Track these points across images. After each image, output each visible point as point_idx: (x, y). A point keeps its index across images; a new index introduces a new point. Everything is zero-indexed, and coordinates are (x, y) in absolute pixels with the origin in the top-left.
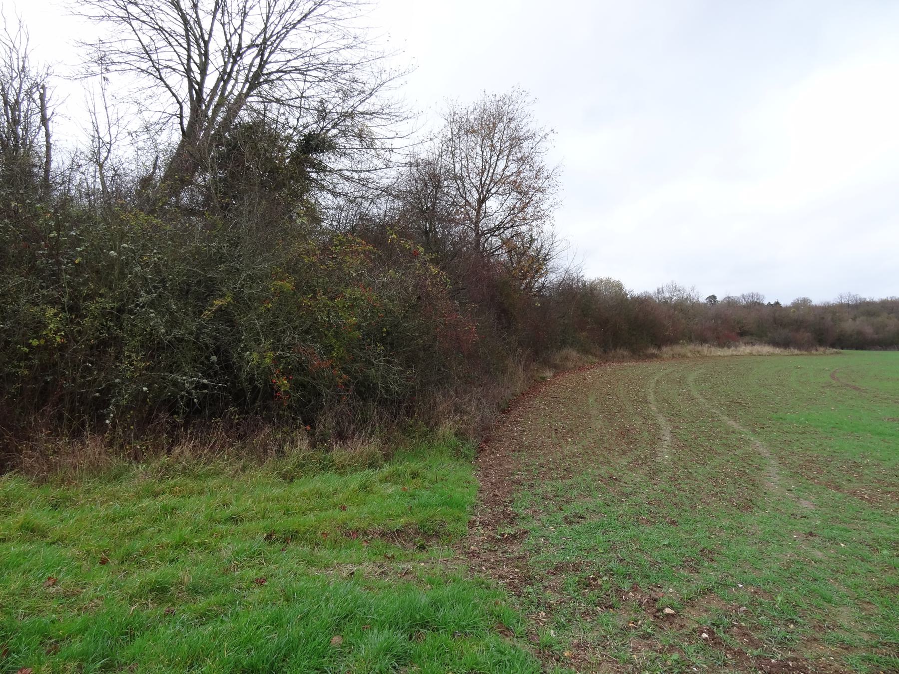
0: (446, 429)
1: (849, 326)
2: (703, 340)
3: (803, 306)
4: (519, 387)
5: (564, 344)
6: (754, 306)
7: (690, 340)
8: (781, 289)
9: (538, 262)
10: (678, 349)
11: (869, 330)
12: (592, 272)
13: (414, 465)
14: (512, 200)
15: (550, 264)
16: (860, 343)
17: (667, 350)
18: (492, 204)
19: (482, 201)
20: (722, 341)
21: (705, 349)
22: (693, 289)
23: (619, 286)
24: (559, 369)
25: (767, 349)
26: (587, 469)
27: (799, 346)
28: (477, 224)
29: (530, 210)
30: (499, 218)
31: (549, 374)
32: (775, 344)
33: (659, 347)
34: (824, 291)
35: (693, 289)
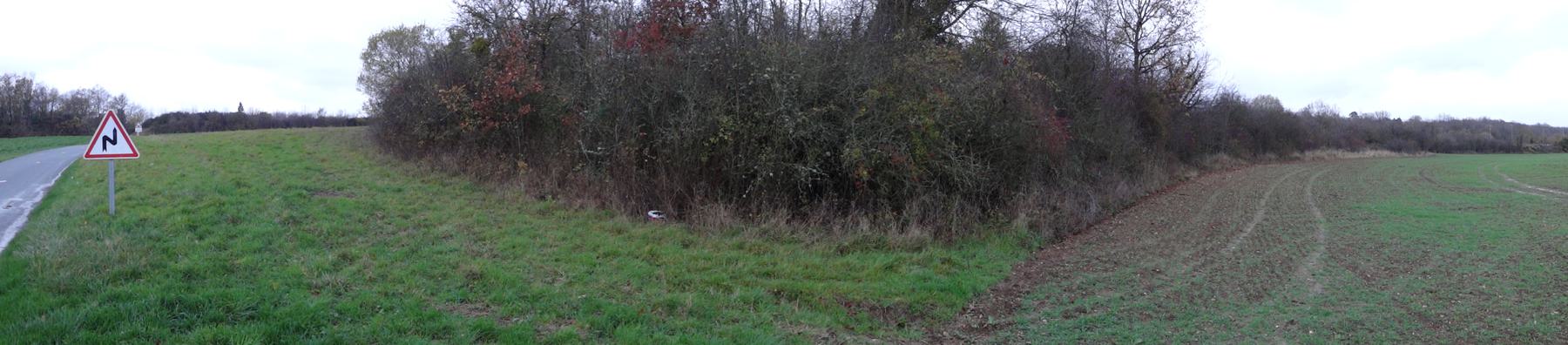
0: (1021, 221)
1: (1441, 136)
2: (1339, 146)
3: (1415, 121)
4: (1155, 185)
5: (1217, 149)
6: (1383, 121)
7: (1329, 146)
8: (1401, 111)
9: (1195, 79)
10: (1318, 153)
11: (1453, 140)
12: (1249, 91)
13: (972, 251)
14: (1165, 22)
15: (1205, 80)
16: (1447, 148)
17: (1309, 154)
18: (1148, 26)
19: (1140, 24)
20: (1353, 146)
21: (1340, 154)
22: (241, 107)
23: (1277, 102)
24: (1204, 170)
25: (1386, 153)
26: (1160, 245)
27: (1408, 150)
28: (1136, 44)
29: (1181, 32)
30: (1154, 37)
31: (1194, 174)
32: (1392, 149)
33: (1302, 151)
34: (1430, 112)
35: (241, 107)
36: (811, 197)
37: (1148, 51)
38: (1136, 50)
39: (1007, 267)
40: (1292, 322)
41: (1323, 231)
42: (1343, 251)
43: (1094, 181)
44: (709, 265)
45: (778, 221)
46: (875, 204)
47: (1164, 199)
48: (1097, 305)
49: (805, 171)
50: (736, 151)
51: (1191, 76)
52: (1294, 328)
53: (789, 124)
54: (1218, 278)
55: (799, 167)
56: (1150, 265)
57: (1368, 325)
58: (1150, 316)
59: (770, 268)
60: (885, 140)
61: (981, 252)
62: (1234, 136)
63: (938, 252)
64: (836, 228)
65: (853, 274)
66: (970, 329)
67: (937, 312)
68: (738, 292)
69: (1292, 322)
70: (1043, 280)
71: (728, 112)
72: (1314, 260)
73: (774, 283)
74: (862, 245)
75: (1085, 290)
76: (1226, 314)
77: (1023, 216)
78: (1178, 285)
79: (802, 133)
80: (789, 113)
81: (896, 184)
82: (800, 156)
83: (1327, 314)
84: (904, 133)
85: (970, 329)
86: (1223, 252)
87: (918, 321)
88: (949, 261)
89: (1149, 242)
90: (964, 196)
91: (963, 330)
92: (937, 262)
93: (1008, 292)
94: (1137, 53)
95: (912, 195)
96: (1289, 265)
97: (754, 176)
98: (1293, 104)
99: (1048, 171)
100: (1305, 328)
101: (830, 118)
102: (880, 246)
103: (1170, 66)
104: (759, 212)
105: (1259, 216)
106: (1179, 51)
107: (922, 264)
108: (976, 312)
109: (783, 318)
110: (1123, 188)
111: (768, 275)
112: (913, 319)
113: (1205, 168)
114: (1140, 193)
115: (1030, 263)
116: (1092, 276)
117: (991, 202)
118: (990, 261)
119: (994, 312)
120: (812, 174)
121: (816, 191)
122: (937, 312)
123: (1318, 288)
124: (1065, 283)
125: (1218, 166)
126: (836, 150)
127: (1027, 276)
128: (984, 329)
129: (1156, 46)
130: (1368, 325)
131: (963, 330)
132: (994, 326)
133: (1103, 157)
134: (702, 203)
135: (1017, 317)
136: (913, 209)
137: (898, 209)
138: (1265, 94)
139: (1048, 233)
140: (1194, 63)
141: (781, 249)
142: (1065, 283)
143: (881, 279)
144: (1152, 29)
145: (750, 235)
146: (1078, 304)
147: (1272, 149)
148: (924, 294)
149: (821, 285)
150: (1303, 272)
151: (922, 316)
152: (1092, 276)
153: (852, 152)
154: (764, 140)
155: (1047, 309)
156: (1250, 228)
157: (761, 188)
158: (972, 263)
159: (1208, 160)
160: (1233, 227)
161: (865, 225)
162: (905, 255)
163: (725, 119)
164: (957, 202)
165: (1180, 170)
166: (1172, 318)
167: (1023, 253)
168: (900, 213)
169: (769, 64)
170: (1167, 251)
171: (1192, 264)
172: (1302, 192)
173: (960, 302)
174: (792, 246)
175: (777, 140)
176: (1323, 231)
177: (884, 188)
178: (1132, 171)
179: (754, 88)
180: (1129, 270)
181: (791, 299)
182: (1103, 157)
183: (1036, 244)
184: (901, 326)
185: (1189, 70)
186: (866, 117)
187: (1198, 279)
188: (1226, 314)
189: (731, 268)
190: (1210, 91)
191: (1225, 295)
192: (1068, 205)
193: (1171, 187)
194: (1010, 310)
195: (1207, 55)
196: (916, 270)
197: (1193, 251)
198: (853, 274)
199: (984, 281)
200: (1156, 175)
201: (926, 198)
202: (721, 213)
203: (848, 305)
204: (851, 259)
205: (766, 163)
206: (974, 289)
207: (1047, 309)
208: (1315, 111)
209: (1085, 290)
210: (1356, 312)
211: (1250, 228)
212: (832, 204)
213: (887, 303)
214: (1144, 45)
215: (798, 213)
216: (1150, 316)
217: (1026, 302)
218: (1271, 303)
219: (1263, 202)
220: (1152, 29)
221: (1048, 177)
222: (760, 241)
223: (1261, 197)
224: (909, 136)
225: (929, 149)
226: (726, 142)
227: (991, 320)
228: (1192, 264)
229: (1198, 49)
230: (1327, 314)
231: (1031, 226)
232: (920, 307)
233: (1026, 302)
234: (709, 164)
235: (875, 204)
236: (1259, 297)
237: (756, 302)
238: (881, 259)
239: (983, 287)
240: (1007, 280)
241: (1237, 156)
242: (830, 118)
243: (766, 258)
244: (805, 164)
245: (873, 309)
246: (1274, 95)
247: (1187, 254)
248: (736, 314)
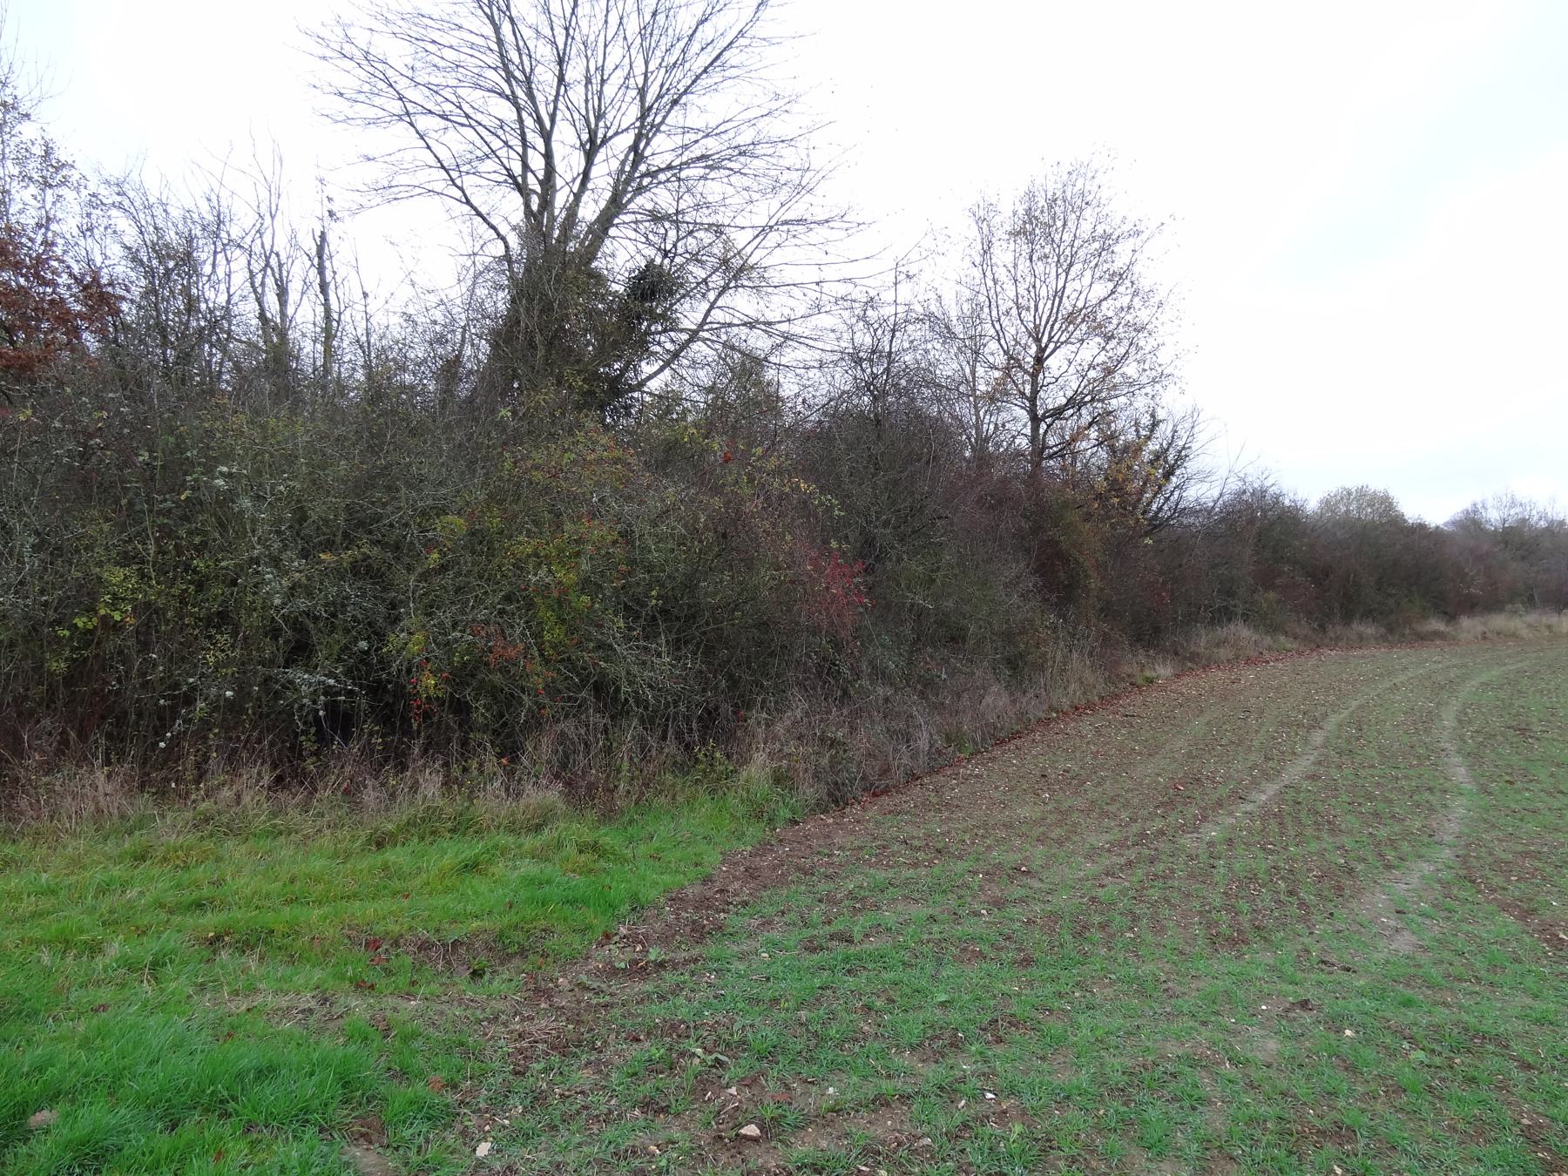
0: (757, 769)
5: (1223, 615)
7: (1530, 602)
10: (1498, 621)
12: (1309, 481)
15: (1192, 466)
17: (1469, 625)
24: (1190, 661)
29: (1130, 369)
31: (1164, 671)
33: (1451, 617)
36: (322, 739)
37: (1058, 413)
38: (1032, 413)
39: (712, 858)
40: (1304, 1004)
41: (1457, 817)
42: (1503, 867)
43: (927, 686)
44: (46, 903)
45: (245, 791)
46: (464, 743)
47: (1086, 726)
48: (877, 929)
49: (308, 683)
50: (145, 647)
51: (1159, 455)
52: (1307, 1018)
53: (274, 586)
54: (1154, 894)
55: (299, 676)
56: (1013, 858)
57: (1518, 1048)
58: (981, 956)
59: (206, 891)
60: (482, 614)
61: (663, 829)
62: (1269, 585)
63: (577, 830)
64: (370, 796)
65: (396, 884)
66: (614, 972)
67: (552, 943)
68: (115, 948)
69: (1304, 1004)
70: (782, 881)
71: (126, 560)
72: (1415, 879)
73: (210, 921)
74: (426, 827)
75: (860, 903)
76: (1149, 968)
77: (760, 757)
78: (1062, 900)
79: (302, 603)
80: (276, 562)
81: (505, 701)
82: (300, 652)
83: (1408, 1003)
84: (519, 600)
85: (614, 972)
86: (1186, 841)
87: (516, 962)
88: (595, 847)
89: (1024, 812)
90: (648, 722)
91: (598, 974)
92: (570, 850)
93: (703, 903)
94: (1035, 420)
95: (536, 723)
96: (1339, 883)
97: (189, 701)
98: (1430, 504)
99: (827, 670)
100: (1335, 1024)
101: (361, 570)
102: (462, 826)
103: (1108, 440)
104: (200, 776)
105: (1295, 771)
106: (1129, 410)
107: (538, 856)
108: (631, 940)
109: (218, 988)
110: (996, 701)
111: (199, 905)
112: (506, 958)
113: (1194, 657)
114: (1037, 711)
115: (763, 848)
116: (882, 875)
117: (702, 731)
118: (681, 840)
119: (665, 940)
120: (328, 691)
121: (340, 721)
122: (552, 943)
123: (1404, 943)
124: (823, 887)
125: (1224, 653)
126: (378, 636)
127: (751, 874)
128: (638, 970)
129: (1074, 402)
130: (1518, 1048)
131: (598, 974)
132: (661, 965)
133: (956, 638)
134: (49, 768)
135: (711, 948)
136: (541, 749)
137: (510, 751)
138: (1353, 483)
139: (810, 792)
140: (1164, 431)
141: (234, 849)
142: (823, 887)
143: (447, 890)
144: (1067, 369)
145: (170, 828)
146: (837, 927)
147: (1369, 614)
148: (529, 912)
149: (316, 913)
150: (1376, 902)
151: (523, 953)
152: (882, 875)
153: (410, 640)
154: (223, 619)
155: (775, 935)
156: (1265, 795)
157: (206, 724)
158: (642, 849)
159: (1202, 640)
160: (1224, 791)
161: (431, 785)
162: (506, 840)
163: (116, 575)
164: (631, 730)
165: (1132, 663)
166: (1027, 962)
167: (754, 832)
168: (514, 760)
169: (227, 457)
170: (1056, 833)
171: (1106, 861)
172: (1431, 717)
173: (600, 924)
174: (266, 844)
175: (251, 622)
176: (1457, 817)
177: (481, 712)
178: (1018, 667)
179: (195, 504)
180: (961, 866)
181: (244, 947)
182: (956, 638)
183: (785, 813)
184: (477, 974)
185: (1153, 446)
186: (443, 568)
187: (1110, 890)
188: (1149, 968)
189: (104, 906)
190: (1208, 480)
191: (1158, 929)
192: (865, 738)
193: (1108, 700)
194: (699, 933)
195: (1195, 411)
196: (528, 868)
197: (1116, 835)
198: (396, 884)
199: (653, 884)
200: (1074, 671)
201: (568, 727)
202: (102, 783)
203: (373, 945)
204: (395, 856)
205: (216, 673)
206: (634, 898)
207: (775, 935)
208: (1493, 517)
209: (860, 903)
210: (1500, 1011)
211: (1265, 795)
212: (368, 750)
213: (453, 933)
214: (1053, 398)
215: (289, 773)
216: (981, 956)
217: (732, 921)
218: (1268, 957)
219: (1318, 737)
220: (1067, 369)
221: (830, 679)
222: (192, 838)
223: (1315, 725)
224: (530, 605)
225: (571, 631)
226: (117, 628)
227: (654, 954)
228: (1106, 861)
229: (1172, 404)
230: (1408, 1003)
231: (778, 779)
232: (519, 936)
233: (732, 921)
234: (69, 680)
235: (464, 743)
236: (1237, 941)
237: (156, 965)
238: (452, 852)
239: (653, 894)
240: (707, 880)
241: (1274, 629)
242: (361, 570)
243: (199, 873)
244: (311, 670)
245: (424, 946)
246: (1377, 485)
247: (1100, 841)
248: (104, 995)
